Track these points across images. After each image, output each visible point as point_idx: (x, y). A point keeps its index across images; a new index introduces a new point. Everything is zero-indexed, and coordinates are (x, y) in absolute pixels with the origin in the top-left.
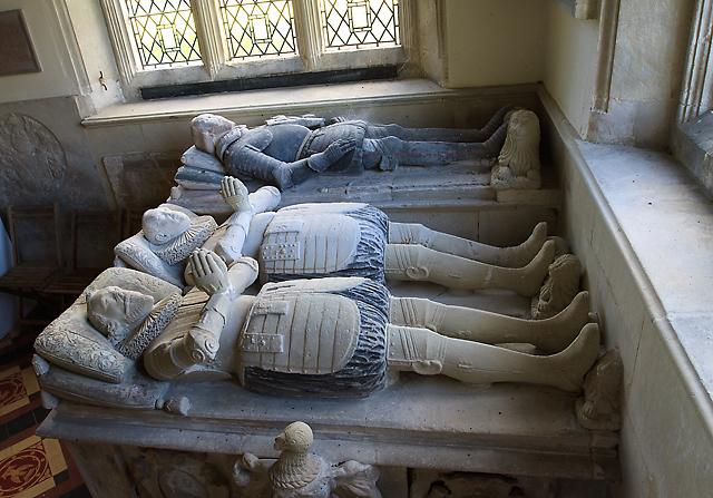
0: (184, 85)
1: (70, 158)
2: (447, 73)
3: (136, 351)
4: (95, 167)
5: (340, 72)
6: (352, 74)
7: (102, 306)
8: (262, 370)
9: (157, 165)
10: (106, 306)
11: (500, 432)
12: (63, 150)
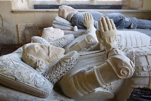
0: (50, 5)
1: (5, 24)
2: (143, 5)
3: (55, 77)
4: (14, 28)
5: (103, 6)
6: (107, 7)
7: (34, 50)
8: (140, 88)
9: (38, 28)
10: (37, 51)
11: (59, 95)
12: (2, 21)
